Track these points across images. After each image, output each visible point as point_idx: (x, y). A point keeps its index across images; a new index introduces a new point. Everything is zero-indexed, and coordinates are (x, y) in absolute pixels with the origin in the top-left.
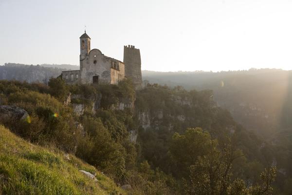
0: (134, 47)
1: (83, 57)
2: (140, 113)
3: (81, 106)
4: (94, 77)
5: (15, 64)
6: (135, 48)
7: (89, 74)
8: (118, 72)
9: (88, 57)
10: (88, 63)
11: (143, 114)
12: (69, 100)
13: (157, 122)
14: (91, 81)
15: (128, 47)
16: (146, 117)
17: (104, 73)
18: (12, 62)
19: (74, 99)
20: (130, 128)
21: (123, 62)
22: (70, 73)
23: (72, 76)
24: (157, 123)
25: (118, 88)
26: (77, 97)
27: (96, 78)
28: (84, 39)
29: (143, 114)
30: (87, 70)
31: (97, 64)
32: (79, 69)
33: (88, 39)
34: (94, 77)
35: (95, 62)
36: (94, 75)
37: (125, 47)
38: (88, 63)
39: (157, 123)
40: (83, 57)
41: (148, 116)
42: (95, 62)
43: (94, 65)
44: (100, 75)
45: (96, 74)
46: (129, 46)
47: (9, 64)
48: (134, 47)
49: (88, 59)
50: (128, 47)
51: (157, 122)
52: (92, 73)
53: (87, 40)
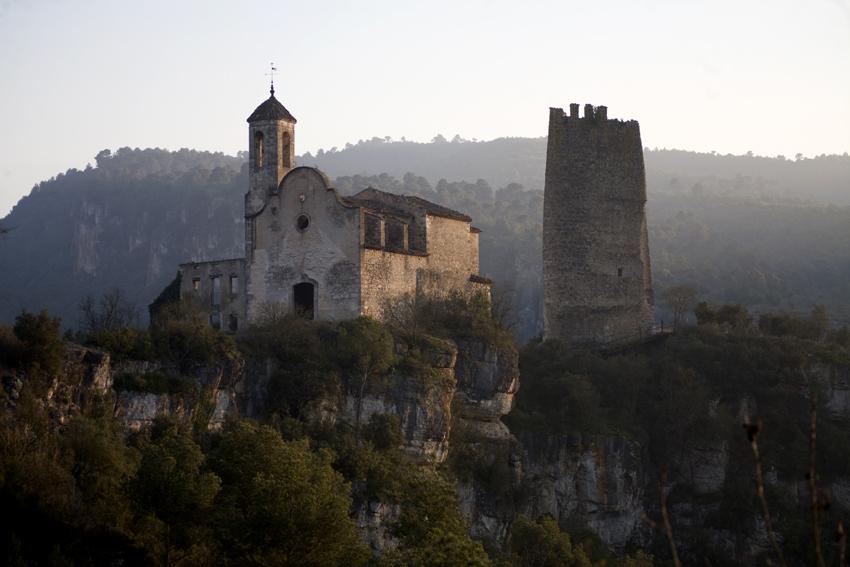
0: (603, 110)
1: (257, 203)
2: (563, 452)
3: (151, 398)
4: (297, 288)
5: (218, 156)
6: (610, 116)
7: (279, 275)
8: (416, 262)
9: (275, 202)
10: (275, 227)
11: (590, 464)
12: (651, 532)
13: (687, 506)
14: (285, 298)
15: (568, 112)
16: (607, 483)
17: (335, 271)
18: (141, 142)
19: (128, 377)
20: (369, 493)
21: (428, 221)
22: (209, 270)
23: (217, 281)
24: (686, 515)
25: (666, 335)
26: (140, 369)
27: (304, 294)
28: (263, 127)
29: (590, 464)
30: (272, 258)
31: (309, 231)
32: (241, 256)
33: (283, 123)
34: (297, 288)
35: (303, 224)
36: (299, 281)
37: (606, 108)
38: (275, 227)
39: (686, 515)
40: (257, 203)
41: (618, 472)
42: (303, 224)
43: (298, 234)
44: (318, 277)
45: (304, 276)
46: (574, 108)
47: (125, 152)
48: (603, 110)
49: (274, 210)
50: (568, 112)
51: (687, 506)
52: (289, 269)
53: (274, 130)
